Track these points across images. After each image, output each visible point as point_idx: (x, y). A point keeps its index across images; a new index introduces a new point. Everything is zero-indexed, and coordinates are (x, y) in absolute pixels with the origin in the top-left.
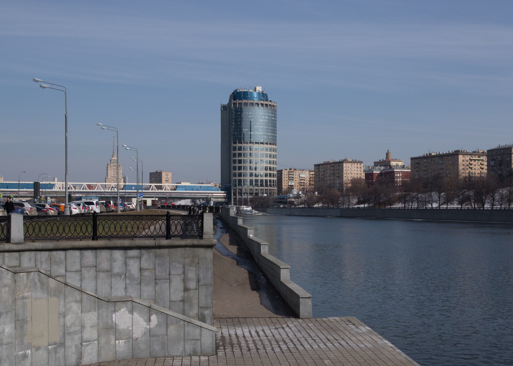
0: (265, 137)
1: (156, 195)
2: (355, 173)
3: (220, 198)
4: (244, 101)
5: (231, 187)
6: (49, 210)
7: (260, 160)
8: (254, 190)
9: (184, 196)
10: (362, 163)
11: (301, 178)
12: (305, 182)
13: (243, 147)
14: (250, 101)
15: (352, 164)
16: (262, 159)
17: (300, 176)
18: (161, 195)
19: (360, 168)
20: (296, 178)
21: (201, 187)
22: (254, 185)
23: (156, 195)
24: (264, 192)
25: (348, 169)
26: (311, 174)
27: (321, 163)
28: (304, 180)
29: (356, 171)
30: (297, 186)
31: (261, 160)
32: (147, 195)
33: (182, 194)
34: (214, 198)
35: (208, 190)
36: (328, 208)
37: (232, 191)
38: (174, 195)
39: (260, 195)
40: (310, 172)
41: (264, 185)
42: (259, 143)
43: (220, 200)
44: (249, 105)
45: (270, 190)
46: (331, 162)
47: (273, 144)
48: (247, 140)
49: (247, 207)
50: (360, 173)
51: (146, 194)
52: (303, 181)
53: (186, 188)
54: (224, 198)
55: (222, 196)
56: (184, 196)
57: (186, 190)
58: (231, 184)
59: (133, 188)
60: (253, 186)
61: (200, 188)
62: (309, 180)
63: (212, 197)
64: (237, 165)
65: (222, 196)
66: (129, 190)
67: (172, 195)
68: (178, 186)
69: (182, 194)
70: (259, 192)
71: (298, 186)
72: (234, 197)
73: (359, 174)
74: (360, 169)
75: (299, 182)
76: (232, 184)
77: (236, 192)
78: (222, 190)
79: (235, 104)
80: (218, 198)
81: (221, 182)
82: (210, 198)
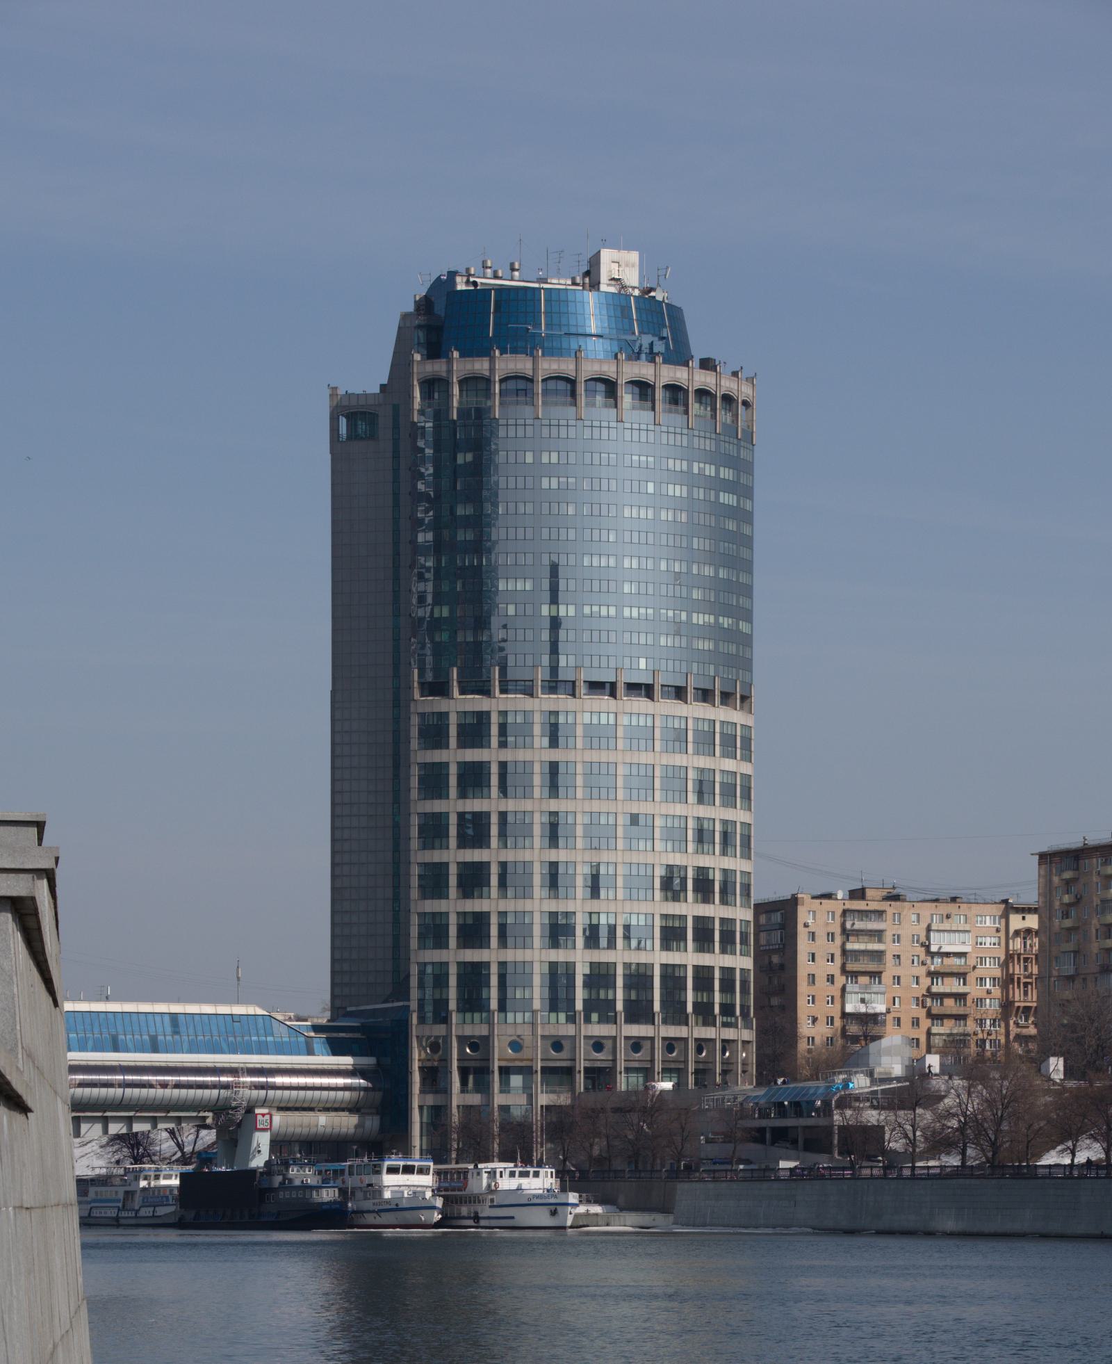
3: (327, 1109)
11: (938, 960)
17: (934, 949)
21: (181, 1018)
22: (579, 1006)
24: (658, 1066)
26: (1017, 933)
28: (962, 976)
31: (634, 819)
34: (280, 1109)
39: (623, 1083)
40: (1005, 916)
41: (657, 1007)
42: (621, 689)
43: (323, 1122)
45: (699, 1050)
49: (524, 1174)
54: (353, 1108)
55: (340, 1094)
60: (571, 1019)
61: (169, 1029)
62: (997, 973)
63: (264, 1103)
64: (453, 855)
65: (336, 1089)
70: (621, 1065)
76: (414, 1005)
77: (446, 1060)
78: (337, 1048)
79: (433, 385)
80: (311, 1109)
82: (250, 1110)
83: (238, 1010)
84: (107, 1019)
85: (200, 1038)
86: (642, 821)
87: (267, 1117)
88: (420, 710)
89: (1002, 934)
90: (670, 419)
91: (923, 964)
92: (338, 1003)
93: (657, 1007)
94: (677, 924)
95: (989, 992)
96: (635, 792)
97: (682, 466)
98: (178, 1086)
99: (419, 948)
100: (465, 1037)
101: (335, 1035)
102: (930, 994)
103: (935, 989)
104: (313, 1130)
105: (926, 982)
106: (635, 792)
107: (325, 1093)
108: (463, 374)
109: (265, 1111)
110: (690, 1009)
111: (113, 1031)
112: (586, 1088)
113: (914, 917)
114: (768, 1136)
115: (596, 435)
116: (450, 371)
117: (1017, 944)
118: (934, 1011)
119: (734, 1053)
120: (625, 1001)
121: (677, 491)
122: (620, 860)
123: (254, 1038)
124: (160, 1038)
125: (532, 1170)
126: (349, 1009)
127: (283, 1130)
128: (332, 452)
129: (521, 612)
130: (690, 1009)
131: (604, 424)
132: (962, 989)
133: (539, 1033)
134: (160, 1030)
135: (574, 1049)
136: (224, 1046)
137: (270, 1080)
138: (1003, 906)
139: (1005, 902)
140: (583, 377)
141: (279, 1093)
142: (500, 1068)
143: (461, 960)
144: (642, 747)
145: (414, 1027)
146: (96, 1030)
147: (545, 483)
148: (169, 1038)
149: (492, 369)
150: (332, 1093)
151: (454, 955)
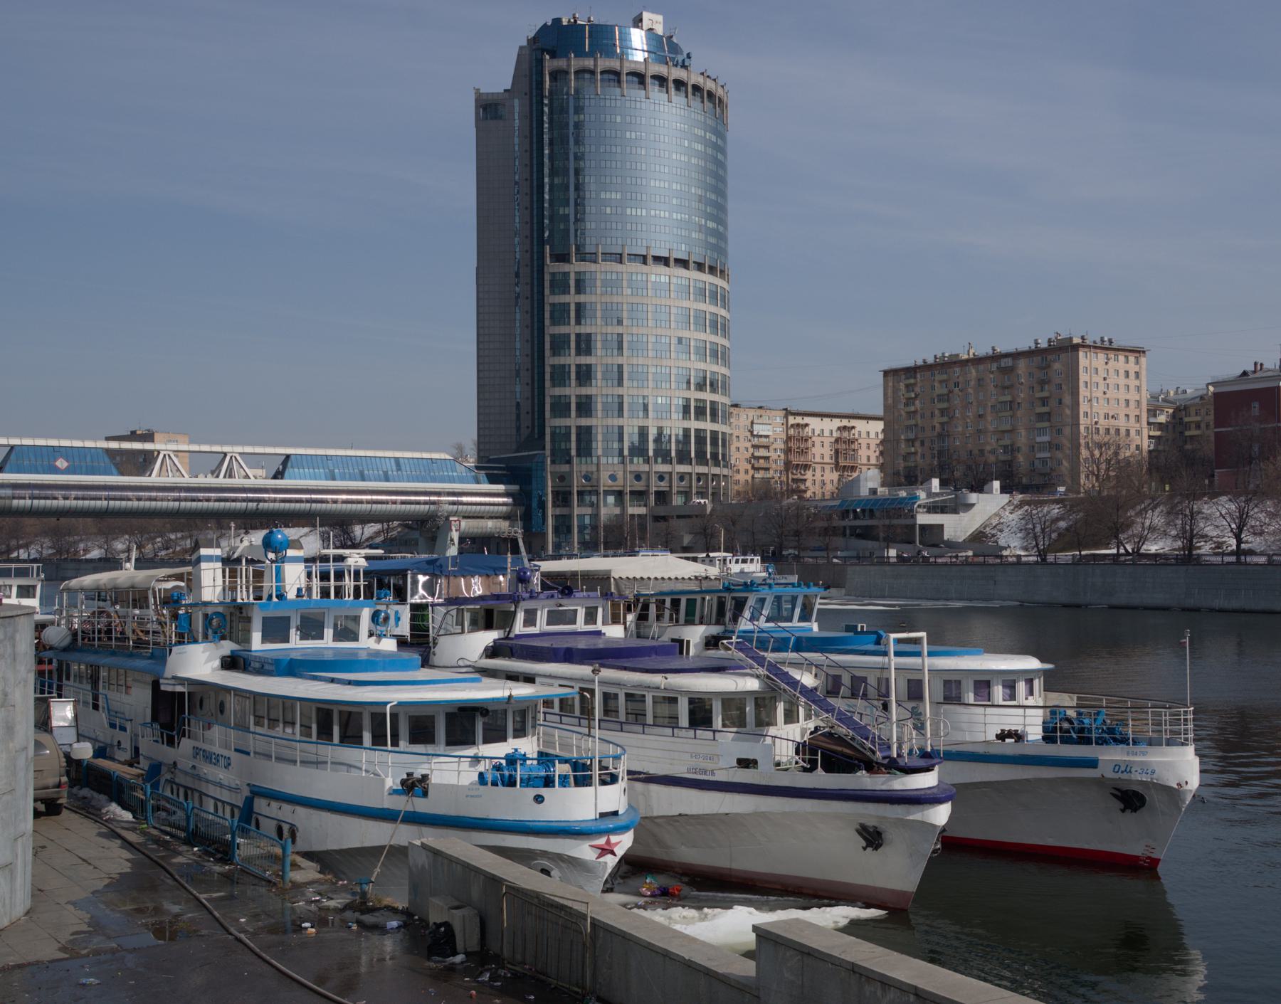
0: (693, 235)
1: (186, 500)
2: (1120, 397)
3: (491, 518)
4: (575, 63)
5: (544, 462)
6: (732, 409)
7: (674, 341)
8: (654, 479)
9: (298, 505)
10: (1144, 352)
11: (756, 439)
12: (773, 455)
13: (572, 276)
14: (603, 63)
15: (1108, 359)
16: (686, 334)
17: (755, 433)
18: (208, 500)
19: (1137, 375)
20: (738, 437)
21: (401, 461)
22: (651, 453)
23: (186, 500)
24: (694, 491)
25: (1095, 379)
26: (792, 426)
27: (1019, 350)
28: (767, 447)
29: (1122, 388)
30: (742, 471)
31: (680, 340)
32: (139, 499)
33: (314, 496)
34: (465, 517)
35: (434, 480)
36: (936, 557)
37: (550, 484)
38: (274, 501)
39: (677, 501)
40: (786, 417)
41: (693, 455)
43: (490, 524)
44: (602, 80)
45: (699, 480)
46: (966, 357)
47: (712, 270)
48: (620, 242)
49: (744, 561)
50: (1138, 398)
51: (130, 494)
52: (762, 453)
53: (331, 468)
54: (506, 517)
55: (501, 508)
56: (298, 505)
57: (334, 479)
58: (544, 448)
59: (61, 463)
60: (647, 461)
61: (394, 468)
62: (782, 446)
63: (455, 514)
65: (498, 504)
66: (38, 473)
67: (264, 500)
68: (292, 457)
69: (314, 496)
70: (675, 490)
71: (747, 472)
72: (558, 511)
73: (1132, 404)
74: (1137, 383)
75: (748, 455)
76: (548, 452)
78: (493, 480)
80: (482, 517)
81: (479, 436)
82: (447, 518)
83: (435, 456)
84: (357, 461)
85: (414, 473)
86: (684, 342)
87: (458, 522)
88: (551, 271)
89: (785, 426)
90: (696, 103)
91: (750, 441)
92: (482, 454)
93: (693, 455)
94: (702, 405)
95: (779, 456)
96: (680, 324)
97: (701, 133)
98: (403, 503)
99: (551, 418)
100: (556, 472)
101: (491, 472)
102: (753, 456)
103: (756, 454)
104: (484, 530)
105: (751, 450)
106: (680, 324)
107: (483, 507)
108: (577, 68)
109: (456, 519)
110: (709, 456)
111: (361, 468)
112: (656, 504)
113: (745, 416)
114: (848, 532)
115: (657, 109)
116: (569, 65)
117: (791, 432)
118: (756, 466)
119: (719, 483)
120: (676, 450)
121: (699, 147)
122: (672, 365)
123: (446, 473)
124: (390, 473)
125: (749, 558)
126: (491, 457)
127: (467, 530)
128: (477, 127)
129: (614, 211)
130: (709, 456)
131: (662, 102)
132: (768, 454)
133: (628, 469)
134: (389, 468)
135: (648, 479)
136: (429, 479)
137: (459, 499)
138: (784, 412)
139: (786, 409)
140: (649, 74)
141: (465, 507)
142: (578, 491)
143: (579, 424)
144: (684, 297)
145: (549, 467)
146: (350, 468)
147: (628, 134)
148: (395, 473)
149: (596, 65)
150: (496, 508)
151: (573, 421)
